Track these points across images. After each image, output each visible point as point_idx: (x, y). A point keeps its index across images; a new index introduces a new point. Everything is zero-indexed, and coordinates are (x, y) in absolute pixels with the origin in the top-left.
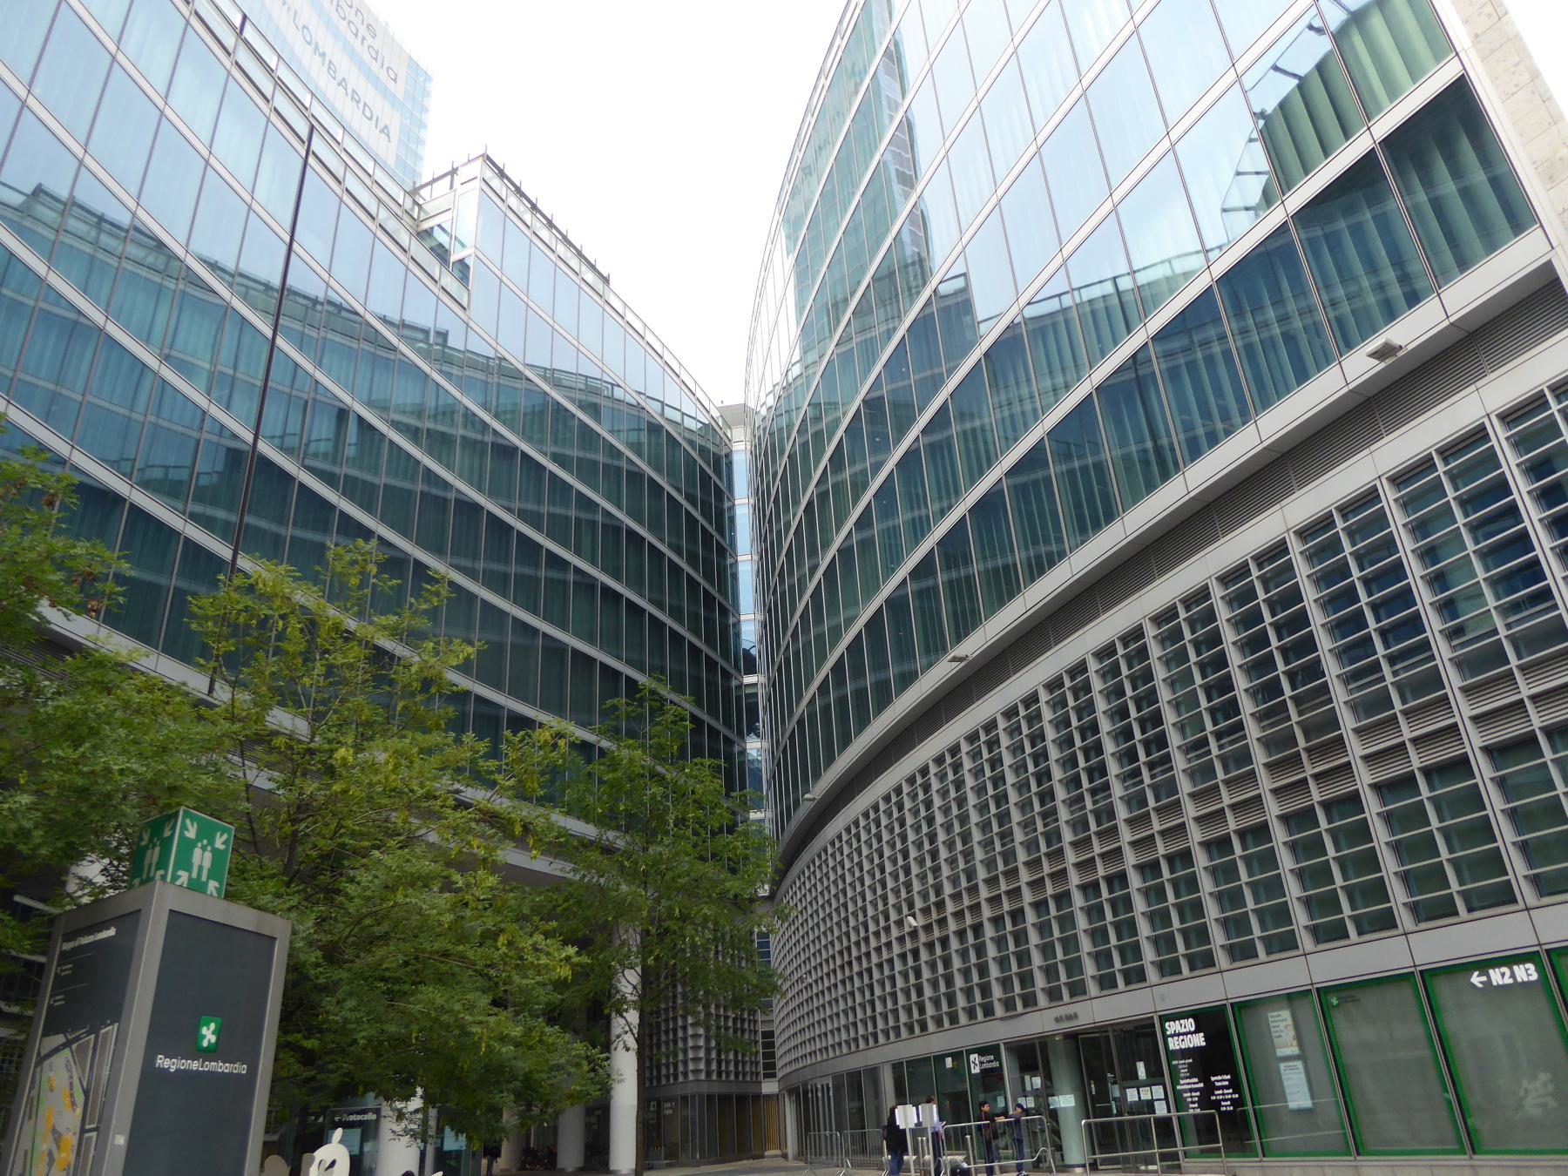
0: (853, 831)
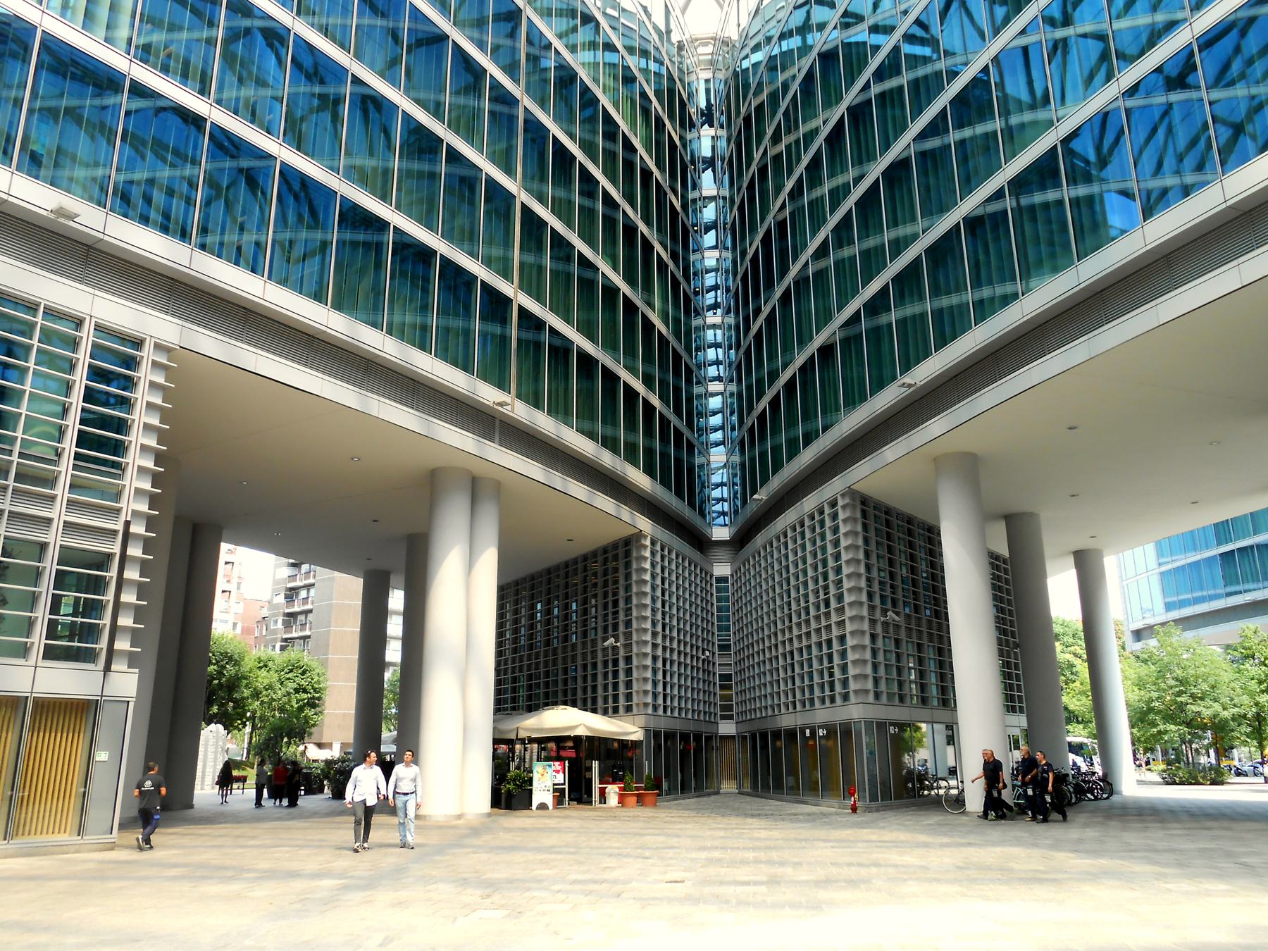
0: (782, 540)
